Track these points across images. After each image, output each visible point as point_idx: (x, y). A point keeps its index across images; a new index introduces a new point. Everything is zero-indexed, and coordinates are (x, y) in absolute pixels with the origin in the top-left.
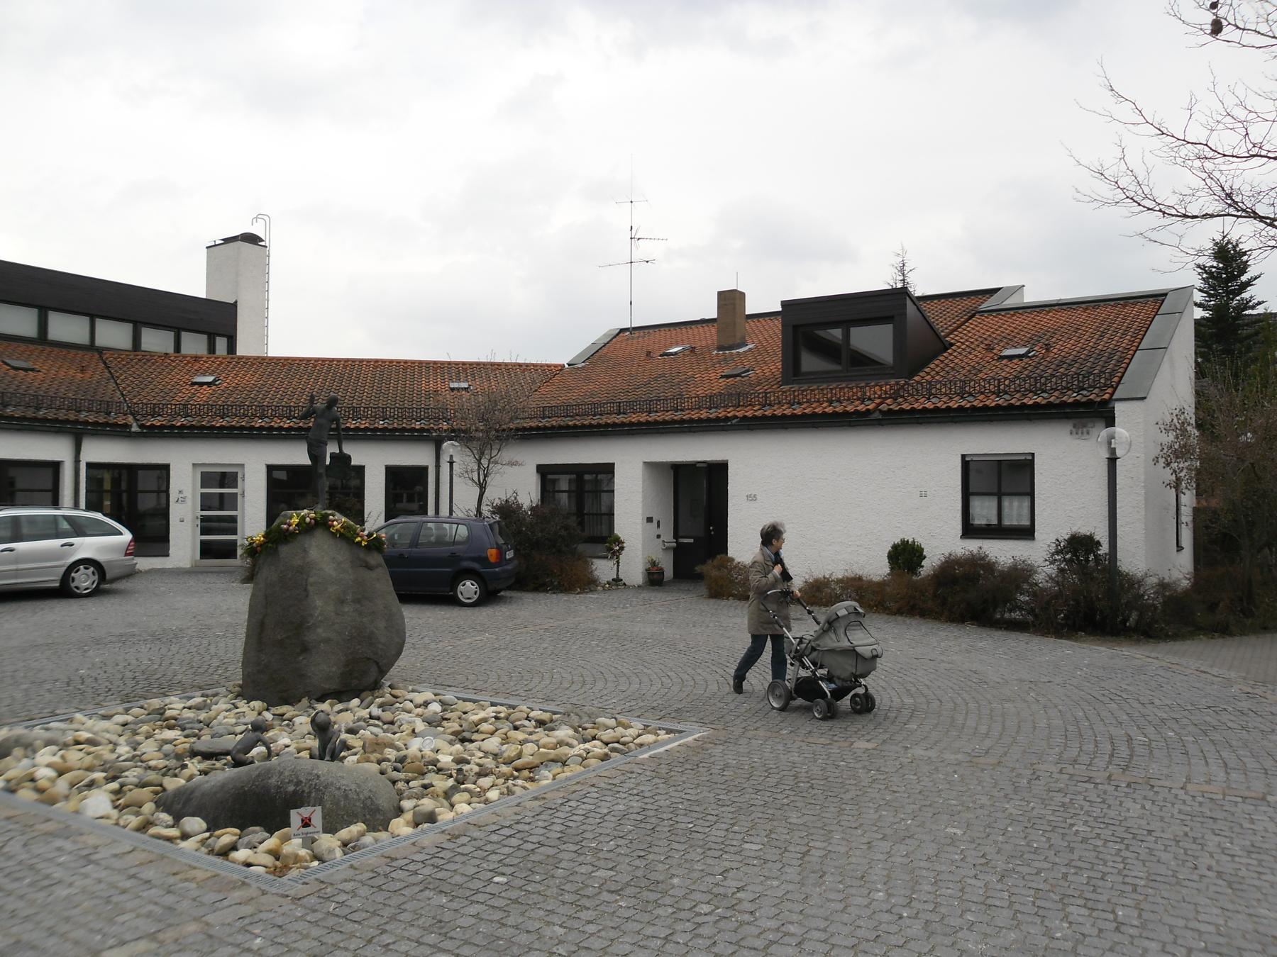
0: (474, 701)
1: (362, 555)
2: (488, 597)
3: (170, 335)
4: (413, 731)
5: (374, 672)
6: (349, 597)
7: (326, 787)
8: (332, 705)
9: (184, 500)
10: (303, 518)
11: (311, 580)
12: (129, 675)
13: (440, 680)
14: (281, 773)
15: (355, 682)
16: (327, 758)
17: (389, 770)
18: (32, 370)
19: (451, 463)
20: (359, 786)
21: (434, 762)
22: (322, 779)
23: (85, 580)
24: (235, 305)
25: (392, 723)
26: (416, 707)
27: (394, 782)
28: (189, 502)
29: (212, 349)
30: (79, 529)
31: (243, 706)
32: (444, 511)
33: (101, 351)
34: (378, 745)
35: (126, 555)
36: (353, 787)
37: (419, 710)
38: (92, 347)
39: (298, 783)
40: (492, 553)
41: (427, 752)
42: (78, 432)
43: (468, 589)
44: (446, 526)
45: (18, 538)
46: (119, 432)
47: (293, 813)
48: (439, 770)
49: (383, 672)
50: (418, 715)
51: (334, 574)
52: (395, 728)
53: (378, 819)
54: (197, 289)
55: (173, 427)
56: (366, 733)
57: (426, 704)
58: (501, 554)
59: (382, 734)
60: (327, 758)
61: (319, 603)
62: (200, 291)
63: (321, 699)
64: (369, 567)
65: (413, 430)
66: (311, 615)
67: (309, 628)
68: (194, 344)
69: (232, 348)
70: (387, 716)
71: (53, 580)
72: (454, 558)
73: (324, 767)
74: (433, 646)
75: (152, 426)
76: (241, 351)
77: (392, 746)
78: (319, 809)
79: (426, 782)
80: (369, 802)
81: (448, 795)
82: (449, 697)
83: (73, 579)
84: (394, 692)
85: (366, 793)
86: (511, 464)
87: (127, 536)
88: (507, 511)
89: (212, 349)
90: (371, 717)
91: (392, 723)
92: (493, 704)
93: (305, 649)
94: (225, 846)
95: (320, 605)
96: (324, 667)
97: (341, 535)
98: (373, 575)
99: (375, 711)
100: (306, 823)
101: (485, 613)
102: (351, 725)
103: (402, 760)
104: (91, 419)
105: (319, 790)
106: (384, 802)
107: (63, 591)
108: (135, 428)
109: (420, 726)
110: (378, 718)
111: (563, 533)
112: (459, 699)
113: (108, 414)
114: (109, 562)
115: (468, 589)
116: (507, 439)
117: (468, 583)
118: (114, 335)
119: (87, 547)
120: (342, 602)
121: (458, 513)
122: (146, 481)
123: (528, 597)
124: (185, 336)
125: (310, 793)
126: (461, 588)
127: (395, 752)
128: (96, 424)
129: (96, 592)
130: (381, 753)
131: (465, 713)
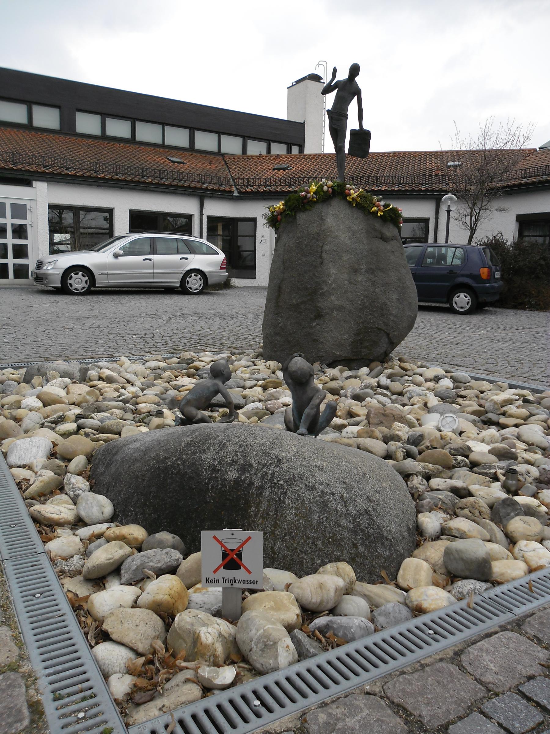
0: (491, 382)
1: (378, 225)
2: (477, 308)
3: (264, 145)
4: (426, 405)
5: (384, 343)
6: (363, 267)
7: (290, 482)
8: (341, 371)
9: (265, 241)
10: (321, 187)
11: (326, 247)
12: (189, 335)
13: (447, 360)
14: (223, 446)
15: (365, 352)
16: (302, 430)
17: (400, 454)
18: (182, 163)
19: (449, 212)
20: (348, 488)
21: (466, 452)
22: (285, 466)
23: (195, 283)
24: (304, 124)
25: (401, 394)
26: (426, 381)
27: (407, 476)
28: (268, 243)
29: (289, 151)
30: (192, 249)
31: (261, 364)
32: (441, 240)
33: (224, 155)
34: (386, 417)
35: (221, 268)
36: (338, 488)
37: (431, 384)
38: (219, 153)
39: (245, 468)
40: (484, 272)
41: (447, 432)
42: (202, 195)
43: (462, 300)
44: (444, 249)
45: (153, 252)
46: (224, 195)
47: (206, 536)
48: (473, 465)
49: (393, 345)
50: (428, 389)
51: (348, 242)
52: (405, 399)
53: (377, 557)
54: (280, 112)
55: (259, 192)
56: (373, 401)
57: (437, 379)
58: (491, 274)
59: (389, 404)
60: (302, 430)
61: (333, 271)
62: (283, 116)
63: (332, 365)
64: (384, 239)
65: (420, 190)
66: (325, 282)
67: (322, 294)
68: (278, 149)
69: (302, 148)
70: (396, 386)
71: (175, 282)
72: (452, 273)
73: (297, 447)
74: (436, 336)
75: (246, 192)
76: (307, 151)
77: (402, 419)
78: (257, 536)
79: (458, 483)
80: (364, 521)
81: (499, 513)
82: (461, 374)
83: (188, 282)
84: (403, 364)
85: (362, 504)
86: (500, 210)
87: (222, 256)
88: (495, 245)
89: (289, 151)
90: (379, 386)
91: (401, 394)
92: (511, 387)
93: (319, 316)
94: (100, 567)
95: (334, 273)
96: (336, 333)
97: (358, 204)
98: (388, 247)
99: (384, 380)
100: (232, 560)
101: (475, 319)
102: (358, 391)
103: (416, 441)
104: (210, 187)
105: (276, 486)
106: (392, 524)
107: (182, 290)
108: (236, 194)
109: (433, 401)
110: (387, 388)
111: (543, 262)
112: (472, 378)
113: (221, 185)
114: (210, 272)
115: (462, 300)
116: (495, 194)
117: (462, 295)
118: (231, 145)
119: (197, 261)
120: (356, 271)
121: (453, 240)
122: (242, 228)
123: (511, 312)
124: (273, 145)
125: (261, 488)
126: (455, 299)
127: (407, 428)
128: (212, 190)
129: (201, 293)
130: (390, 427)
131: (482, 392)
